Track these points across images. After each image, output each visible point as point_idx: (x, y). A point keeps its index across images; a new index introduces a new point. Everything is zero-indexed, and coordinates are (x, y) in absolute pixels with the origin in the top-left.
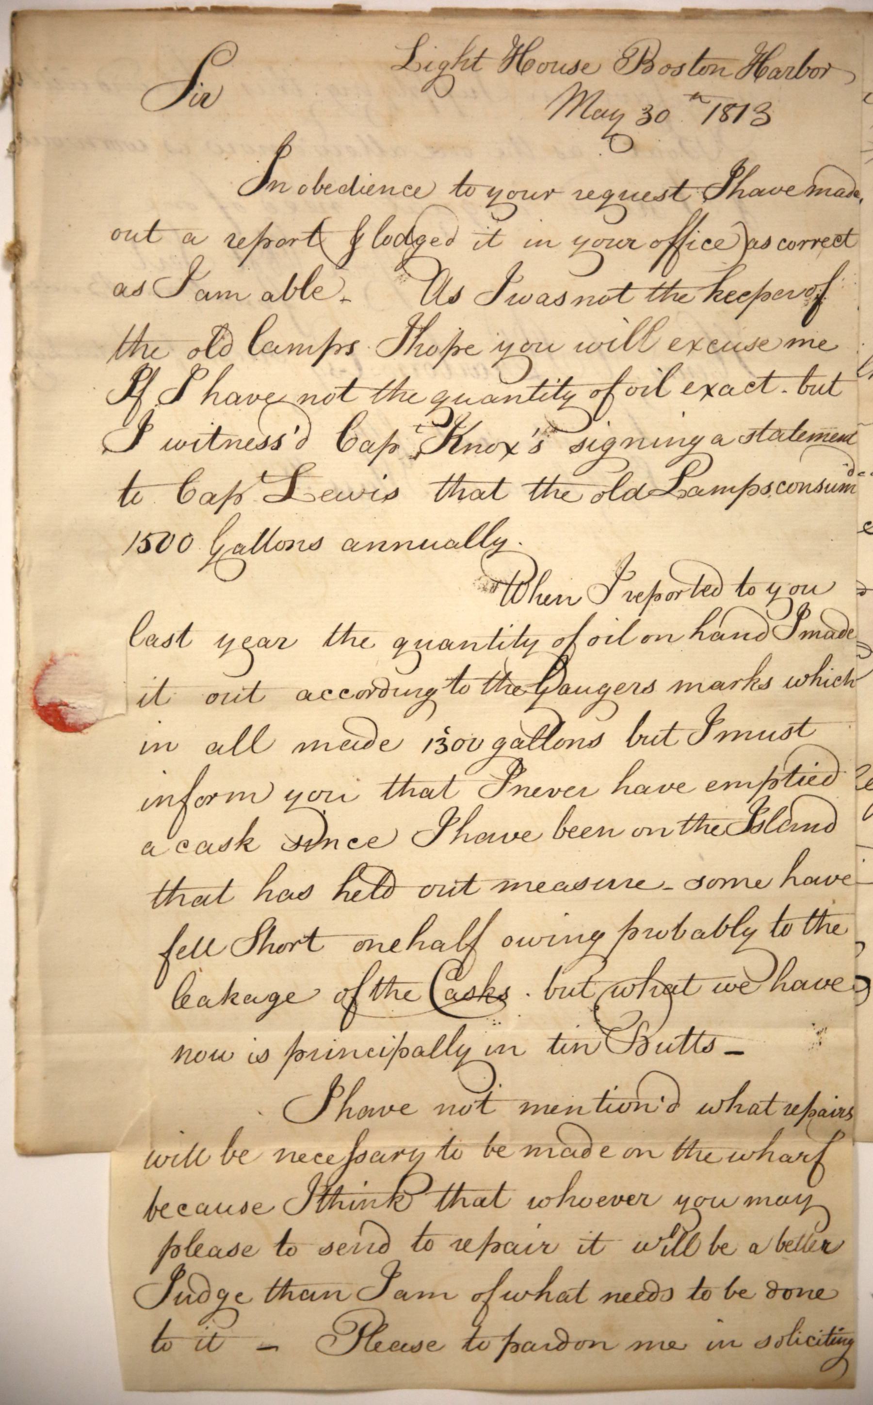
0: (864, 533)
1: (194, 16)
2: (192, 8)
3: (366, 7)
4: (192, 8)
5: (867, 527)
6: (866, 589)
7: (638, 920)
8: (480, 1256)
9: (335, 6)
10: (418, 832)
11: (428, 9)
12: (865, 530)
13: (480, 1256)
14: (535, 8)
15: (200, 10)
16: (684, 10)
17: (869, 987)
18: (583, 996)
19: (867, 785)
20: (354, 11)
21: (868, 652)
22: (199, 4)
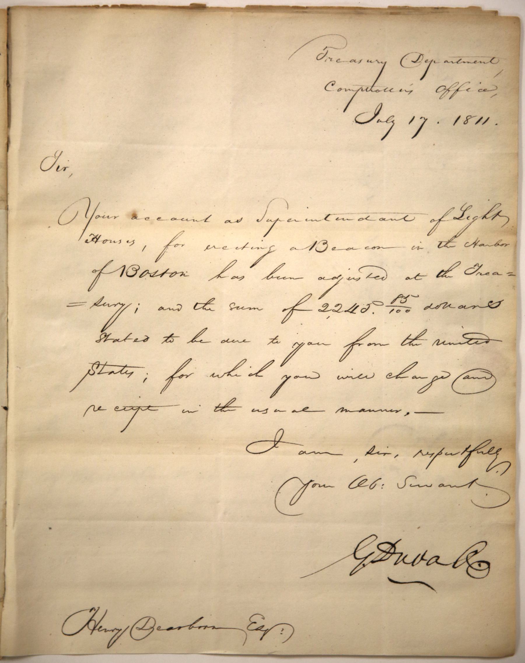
0: (488, 308)
1: (110, 10)
2: (110, 5)
3: (209, 5)
4: (110, 5)
5: (490, 304)
6: (489, 340)
7: (102, 622)
8: (198, 621)
9: (191, 4)
10: (352, 248)
11: (244, 6)
12: (489, 306)
13: (198, 621)
14: (305, 6)
15: (114, 6)
16: (390, 7)
17: (489, 567)
18: (404, 562)
19: (489, 452)
20: (201, 7)
21: (490, 376)
22: (115, 3)
